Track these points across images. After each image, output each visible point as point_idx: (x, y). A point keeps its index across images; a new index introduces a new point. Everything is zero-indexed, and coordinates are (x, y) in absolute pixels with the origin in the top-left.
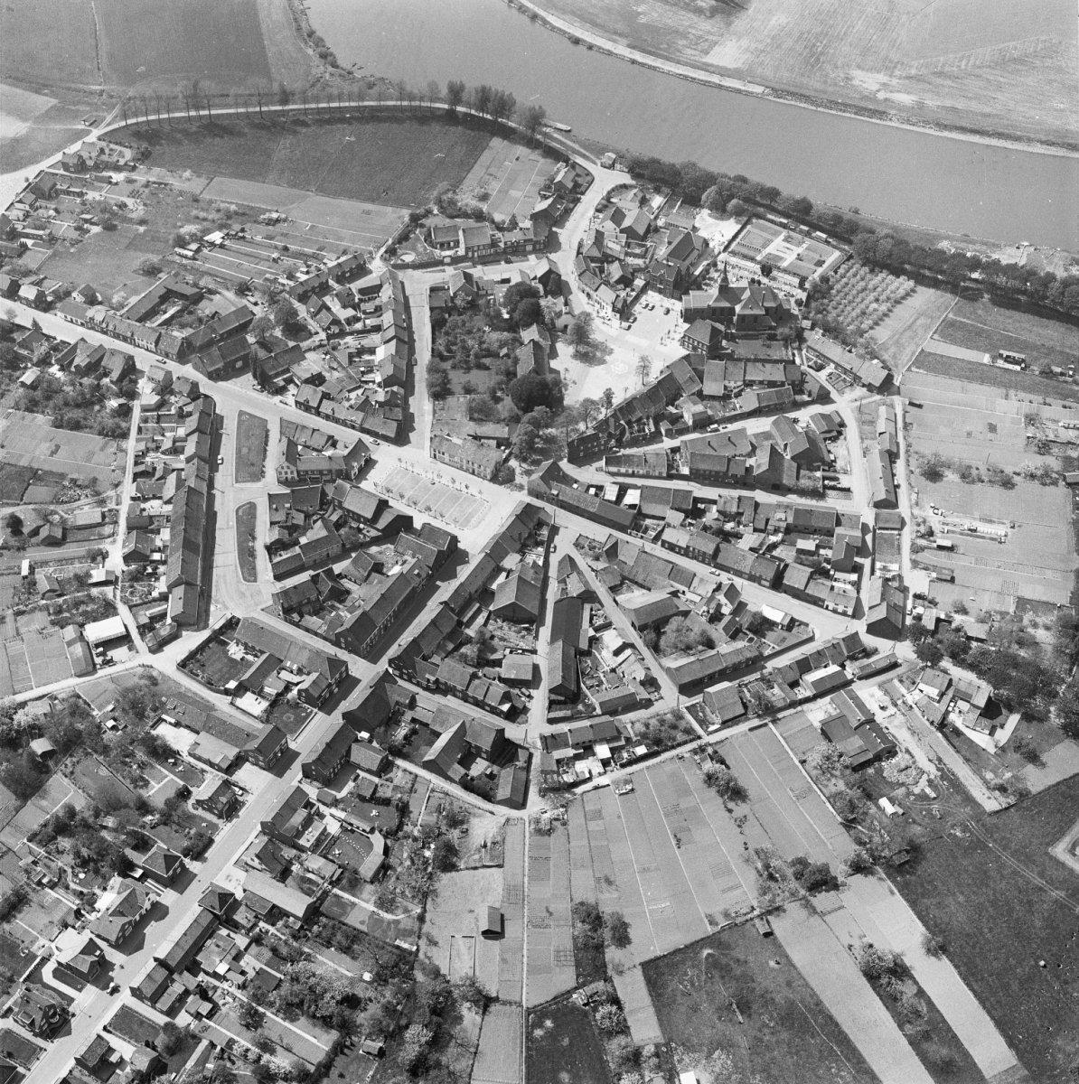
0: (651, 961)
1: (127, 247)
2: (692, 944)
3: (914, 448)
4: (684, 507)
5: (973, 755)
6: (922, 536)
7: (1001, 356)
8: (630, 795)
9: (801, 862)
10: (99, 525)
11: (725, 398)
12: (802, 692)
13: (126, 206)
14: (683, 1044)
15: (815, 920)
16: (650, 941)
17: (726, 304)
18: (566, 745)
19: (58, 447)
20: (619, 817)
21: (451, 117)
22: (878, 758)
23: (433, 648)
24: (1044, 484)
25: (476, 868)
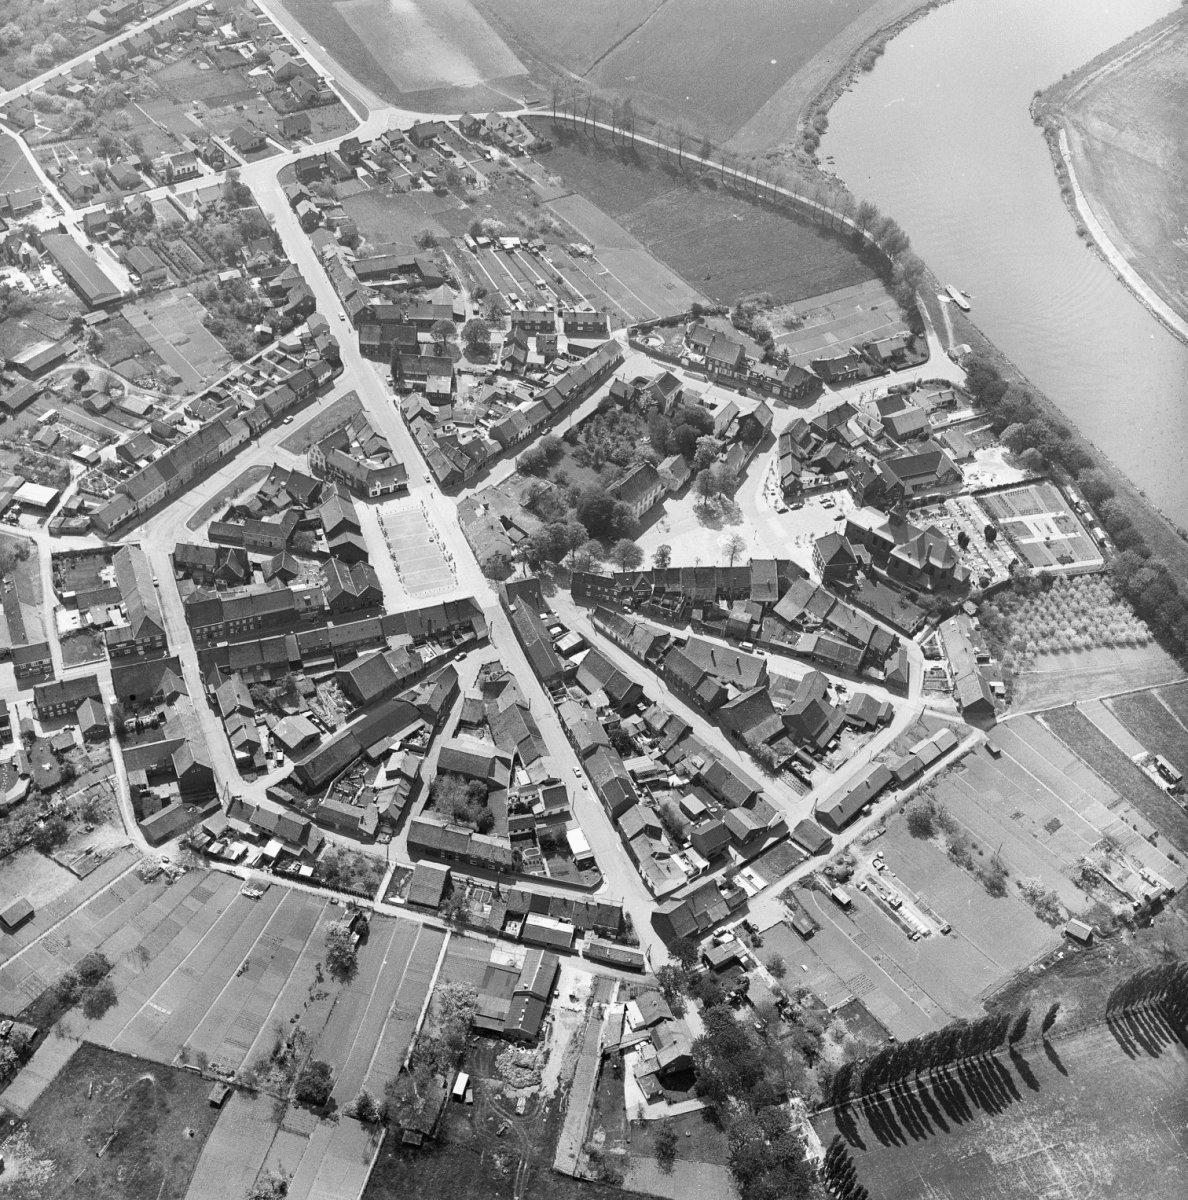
0: (96, 1047)
1: (434, 216)
2: (144, 1060)
3: (936, 791)
4: (616, 694)
5: (607, 1103)
6: (830, 876)
7: (1156, 760)
8: (251, 901)
9: (323, 1070)
10: (139, 417)
11: (794, 626)
12: (514, 929)
13: (474, 181)
14: (33, 1132)
15: (271, 1127)
16: (114, 1032)
17: (889, 538)
18: (247, 820)
19: (188, 341)
20: (220, 912)
21: (855, 242)
22: (511, 1037)
23: (245, 665)
24: (1039, 915)
25: (61, 865)
